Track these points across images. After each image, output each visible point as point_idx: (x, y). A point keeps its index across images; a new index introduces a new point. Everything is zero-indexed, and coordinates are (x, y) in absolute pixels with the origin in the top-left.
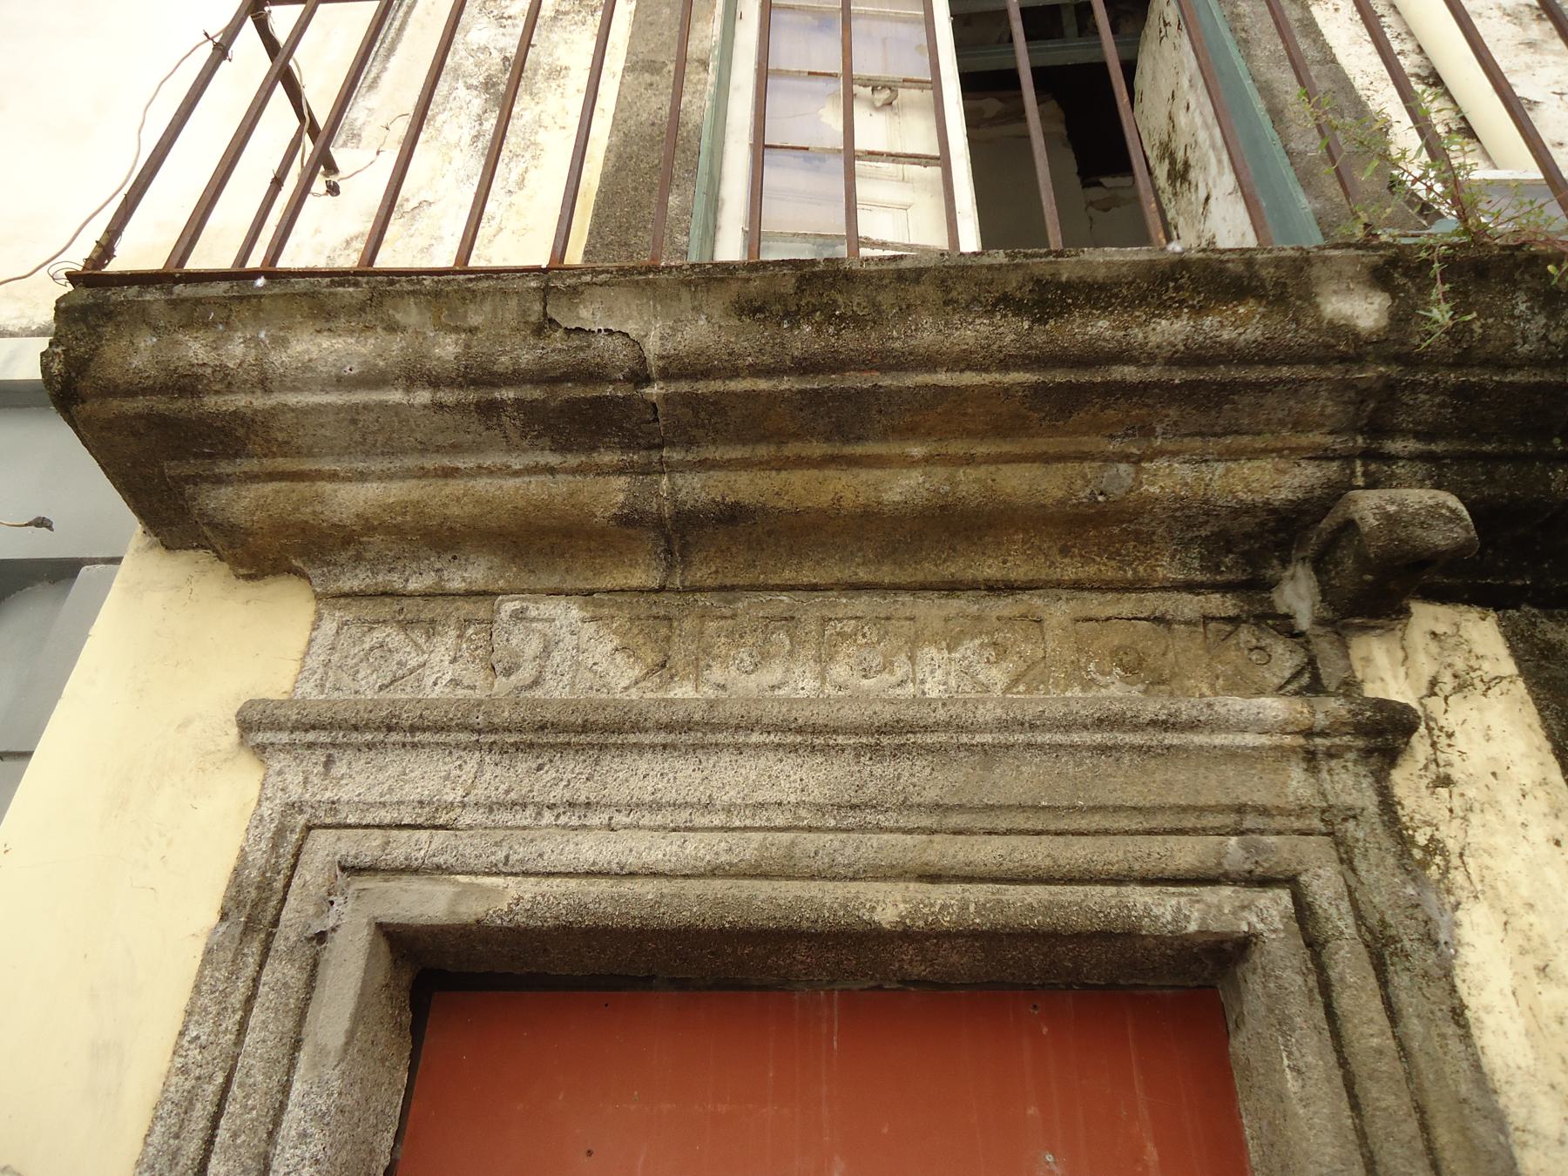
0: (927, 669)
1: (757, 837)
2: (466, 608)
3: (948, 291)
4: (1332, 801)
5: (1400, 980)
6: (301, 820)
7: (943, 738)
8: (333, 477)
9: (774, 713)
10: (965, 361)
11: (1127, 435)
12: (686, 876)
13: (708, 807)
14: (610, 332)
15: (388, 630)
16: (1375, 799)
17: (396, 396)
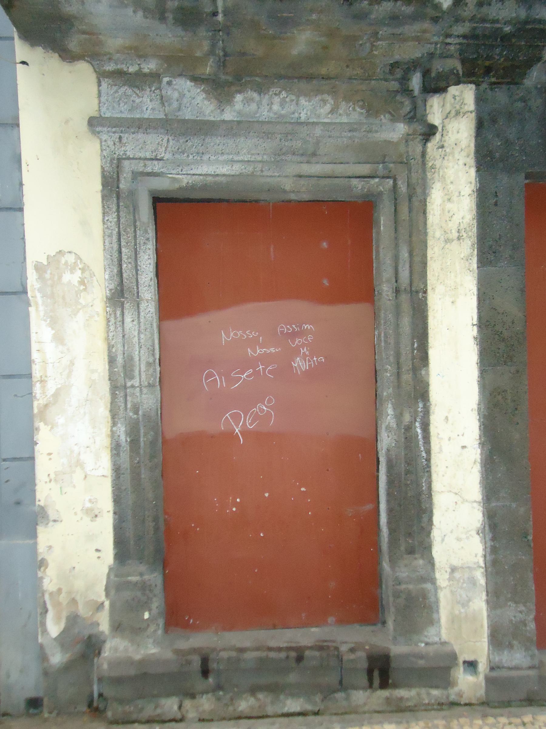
0: (302, 109)
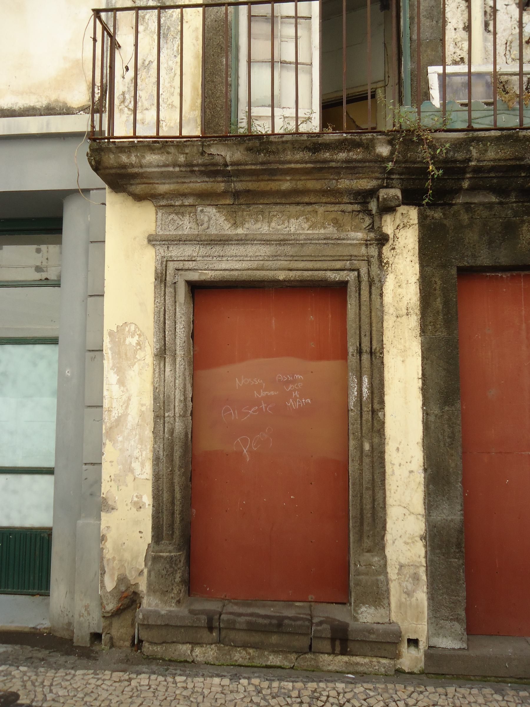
1: (256, 262)
2: (190, 209)
3: (294, 145)
4: (369, 254)
5: (373, 288)
6: (165, 259)
7: (293, 242)
8: (158, 183)
9: (259, 237)
10: (297, 162)
11: (335, 174)
12: (243, 270)
13: (246, 256)
14: (218, 155)
15: (173, 215)
16: (377, 254)
17: (171, 169)
